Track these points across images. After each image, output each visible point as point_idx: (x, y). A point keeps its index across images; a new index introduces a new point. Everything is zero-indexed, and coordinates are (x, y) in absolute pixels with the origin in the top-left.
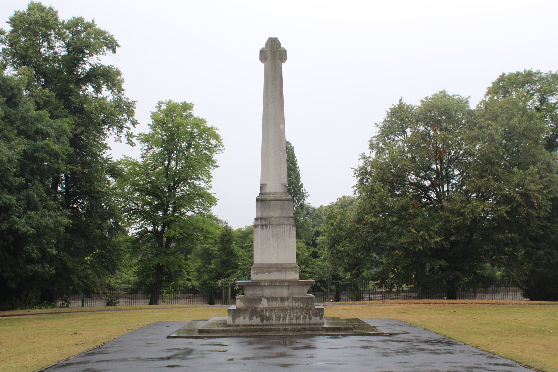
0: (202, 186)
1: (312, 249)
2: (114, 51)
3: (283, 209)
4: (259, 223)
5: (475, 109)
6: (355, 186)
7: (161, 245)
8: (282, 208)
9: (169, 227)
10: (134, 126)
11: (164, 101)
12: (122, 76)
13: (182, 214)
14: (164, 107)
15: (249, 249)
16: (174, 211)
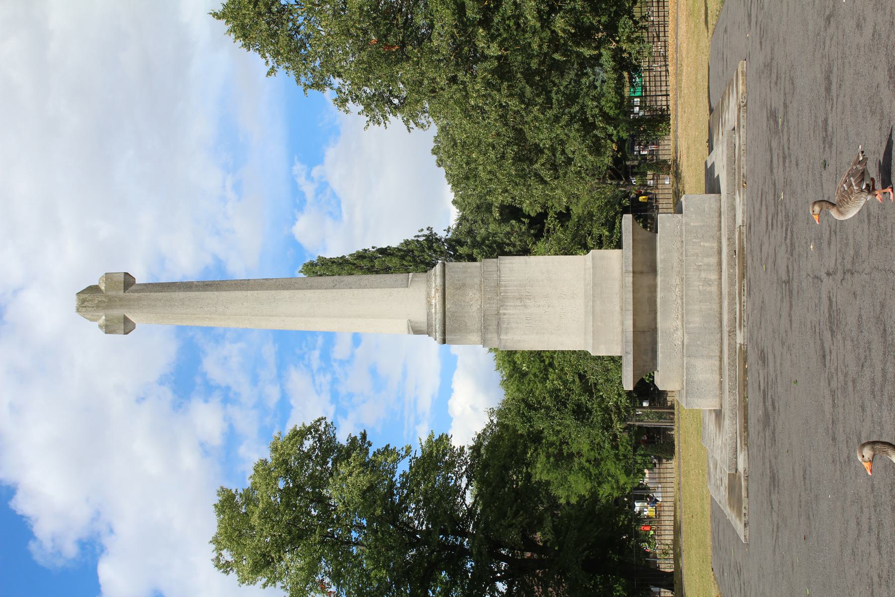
1: (550, 222)
3: (464, 285)
6: (406, 122)
7: (540, 564)
11: (215, 555)
13: (471, 512)
14: (227, 556)
15: (544, 360)
16: (464, 534)
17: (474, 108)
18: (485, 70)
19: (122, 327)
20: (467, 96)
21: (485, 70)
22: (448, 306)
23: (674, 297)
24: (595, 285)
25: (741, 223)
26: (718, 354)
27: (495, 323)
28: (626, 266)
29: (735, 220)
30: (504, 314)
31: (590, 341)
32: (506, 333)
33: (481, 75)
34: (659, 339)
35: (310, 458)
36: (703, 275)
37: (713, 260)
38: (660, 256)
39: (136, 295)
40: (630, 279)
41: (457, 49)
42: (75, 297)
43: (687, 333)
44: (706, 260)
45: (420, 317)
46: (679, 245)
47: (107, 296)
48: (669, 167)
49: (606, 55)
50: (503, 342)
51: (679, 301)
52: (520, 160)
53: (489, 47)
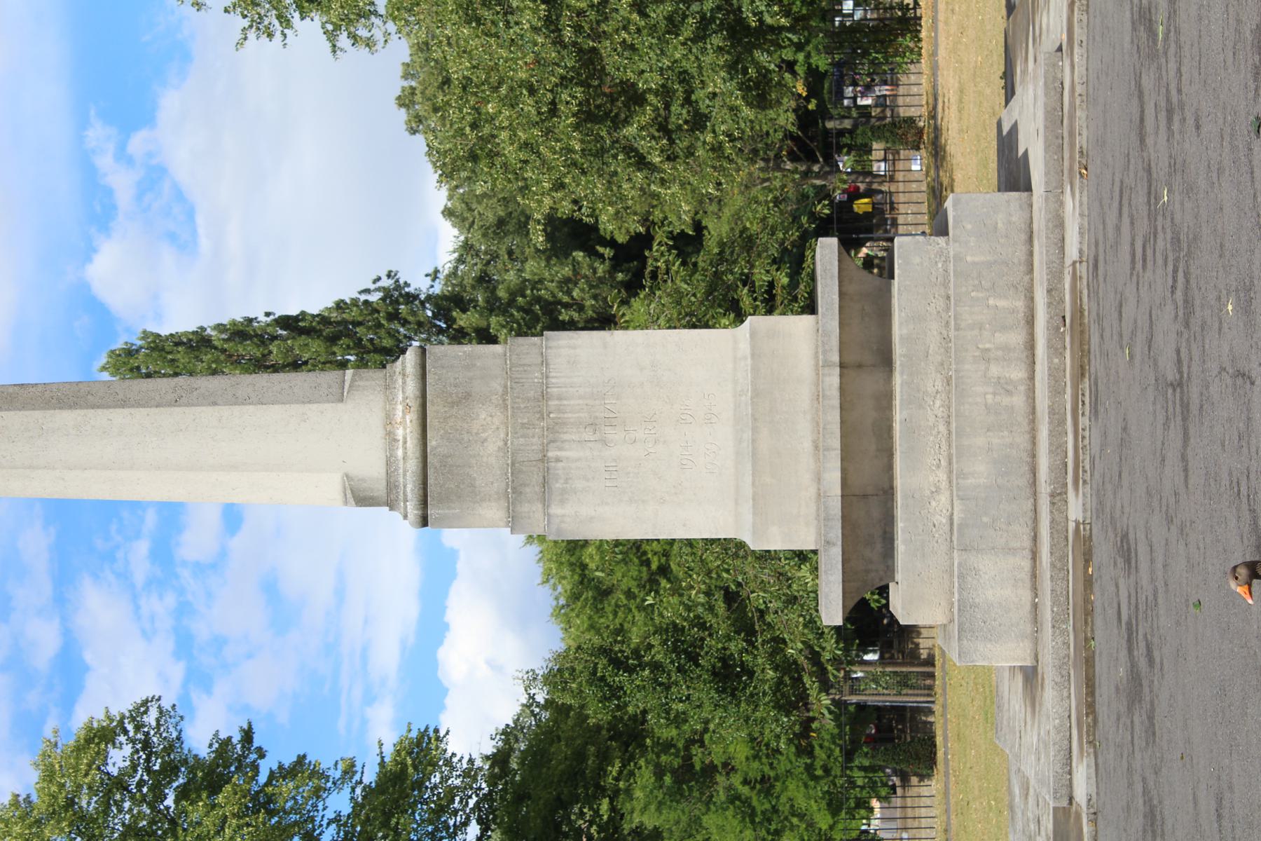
0: (346, 809)
3: (468, 396)
5: (140, 343)
6: (332, 37)
8: (465, 398)
15: (652, 562)
22: (432, 443)
23: (932, 419)
24: (756, 394)
26: (1027, 543)
27: (536, 478)
28: (825, 352)
30: (558, 460)
31: (748, 517)
32: (562, 502)
34: (900, 513)
36: (995, 370)
37: (1016, 338)
38: (899, 329)
40: (833, 379)
44: (1000, 338)
46: (941, 303)
51: (942, 428)
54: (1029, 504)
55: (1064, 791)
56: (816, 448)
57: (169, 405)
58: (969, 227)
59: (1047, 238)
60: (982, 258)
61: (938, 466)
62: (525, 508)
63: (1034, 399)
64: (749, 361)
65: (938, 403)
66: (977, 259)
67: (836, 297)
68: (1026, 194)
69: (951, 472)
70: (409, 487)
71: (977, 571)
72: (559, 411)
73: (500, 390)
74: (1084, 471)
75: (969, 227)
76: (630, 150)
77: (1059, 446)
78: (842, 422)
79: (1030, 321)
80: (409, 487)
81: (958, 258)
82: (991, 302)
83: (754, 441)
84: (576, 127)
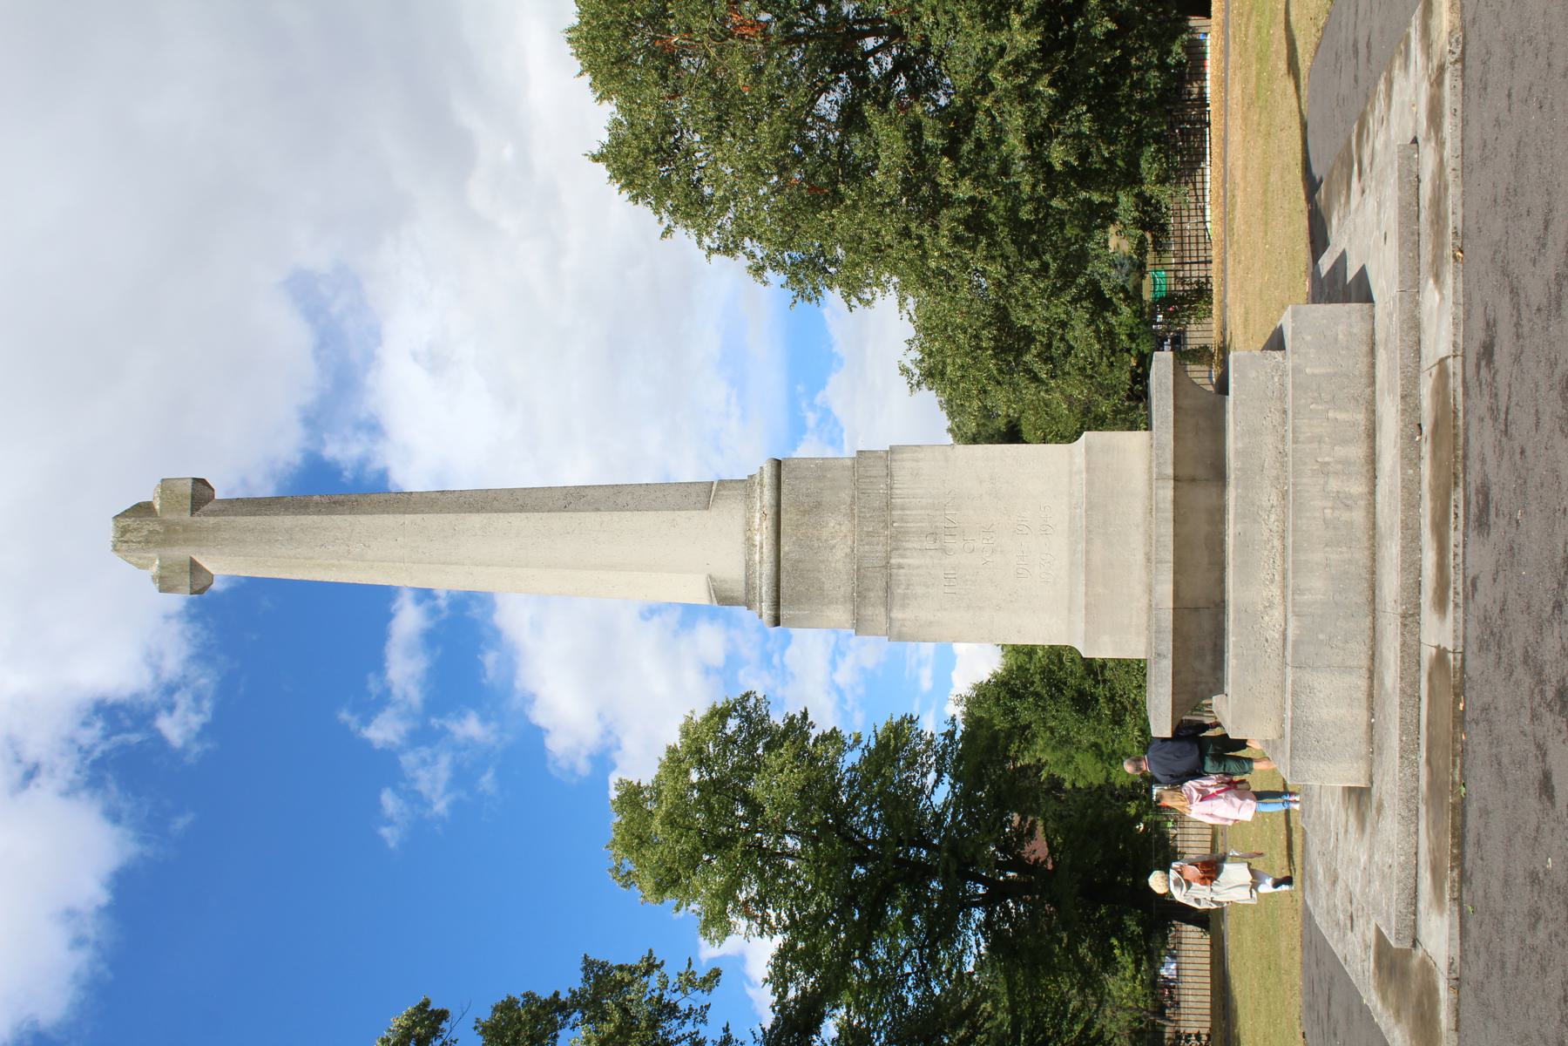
2: (442, 1015)
3: (819, 505)
4: (875, 613)
6: (846, 298)
9: (973, 862)
10: (659, 967)
12: (518, 995)
13: (938, 818)
16: (927, 844)
17: (939, 272)
18: (953, 219)
19: (188, 580)
20: (924, 256)
21: (953, 219)
22: (785, 549)
23: (1266, 534)
24: (1091, 507)
25: (1444, 349)
26: (1365, 662)
27: (880, 584)
28: (1159, 465)
29: (1418, 352)
30: (900, 567)
31: (1080, 626)
32: (903, 606)
33: (945, 226)
34: (1231, 626)
35: (735, 742)
36: (1334, 484)
37: (1357, 452)
38: (1233, 443)
39: (212, 520)
40: (1167, 492)
41: (909, 187)
42: (111, 524)
43: (1296, 614)
44: (1340, 451)
45: (732, 571)
46: (1277, 417)
47: (162, 522)
48: (1212, 356)
49: (1125, 200)
50: (897, 624)
51: (1277, 543)
52: (1003, 351)
53: (956, 186)
54: (1368, 622)
55: (1408, 932)
56: (1149, 560)
57: (560, 510)
58: (1309, 338)
59: (1402, 340)
60: (1323, 371)
61: (1272, 581)
62: (868, 612)
63: (1374, 514)
64: (1084, 475)
65: (1273, 517)
66: (1316, 371)
67: (1171, 411)
68: (1367, 305)
69: (1284, 587)
70: (764, 589)
71: (1312, 689)
72: (902, 520)
73: (848, 500)
74: (1456, 593)
75: (1309, 338)
76: (1028, 371)
77: (1413, 563)
78: (1175, 535)
79: (1372, 434)
80: (764, 589)
81: (1297, 370)
82: (1331, 414)
83: (1087, 552)
84: (994, 356)
